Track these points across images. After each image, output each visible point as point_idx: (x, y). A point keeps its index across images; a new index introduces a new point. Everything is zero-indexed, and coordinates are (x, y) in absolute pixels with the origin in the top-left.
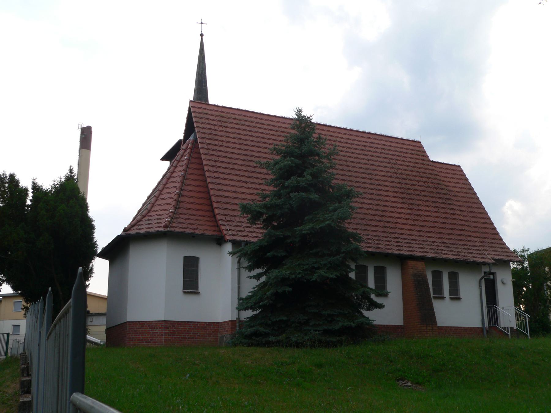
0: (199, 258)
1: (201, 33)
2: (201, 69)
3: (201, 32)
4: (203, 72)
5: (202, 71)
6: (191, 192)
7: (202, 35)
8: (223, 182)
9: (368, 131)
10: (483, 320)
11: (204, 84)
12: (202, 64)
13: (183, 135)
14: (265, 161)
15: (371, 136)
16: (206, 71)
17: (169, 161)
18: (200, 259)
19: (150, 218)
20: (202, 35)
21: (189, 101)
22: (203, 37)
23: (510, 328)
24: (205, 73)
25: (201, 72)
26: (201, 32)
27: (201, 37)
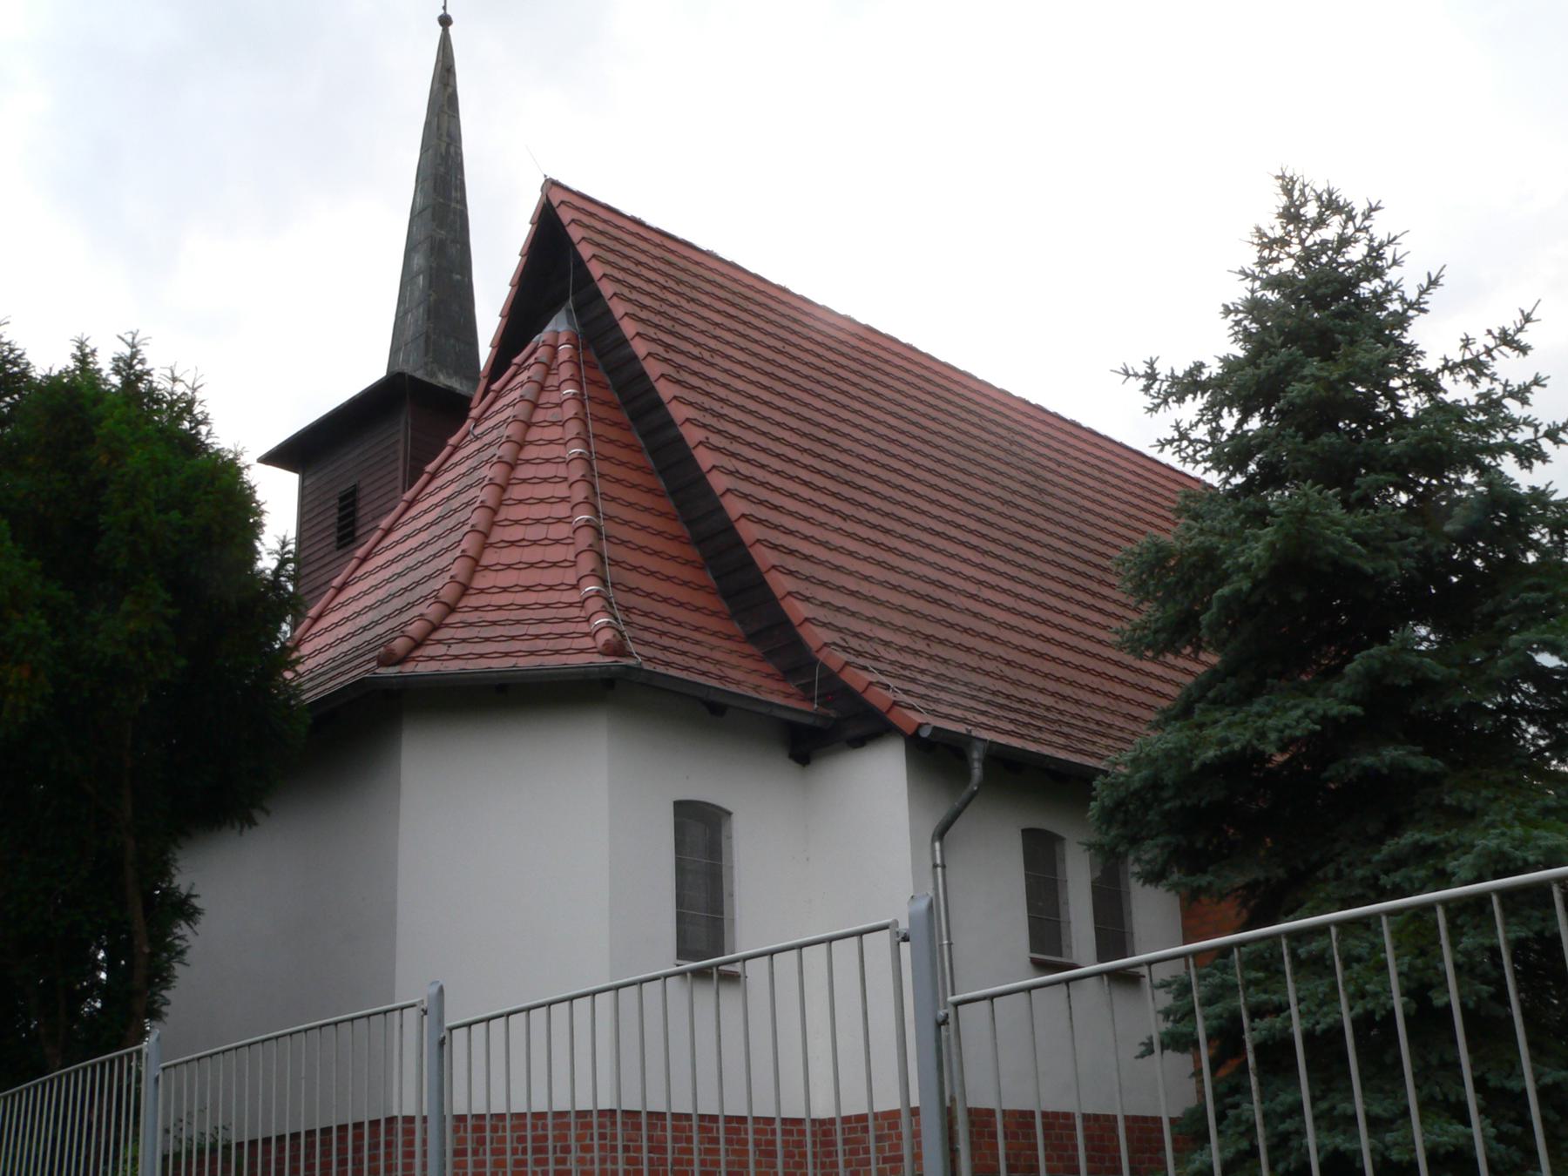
0: (729, 814)
1: (442, 12)
2: (445, 138)
3: (444, 8)
4: (452, 149)
5: (448, 145)
6: (630, 530)
7: (445, 21)
8: (777, 499)
9: (1085, 424)
10: (1201, 1092)
11: (453, 194)
12: (449, 122)
13: (499, 319)
14: (446, 577)
15: (1097, 440)
16: (460, 148)
17: (295, 471)
18: (734, 817)
19: (473, 617)
20: (445, 21)
21: (543, 180)
22: (451, 29)
23: (1127, 1118)
24: (459, 154)
25: (443, 146)
26: (444, 8)
27: (441, 28)
